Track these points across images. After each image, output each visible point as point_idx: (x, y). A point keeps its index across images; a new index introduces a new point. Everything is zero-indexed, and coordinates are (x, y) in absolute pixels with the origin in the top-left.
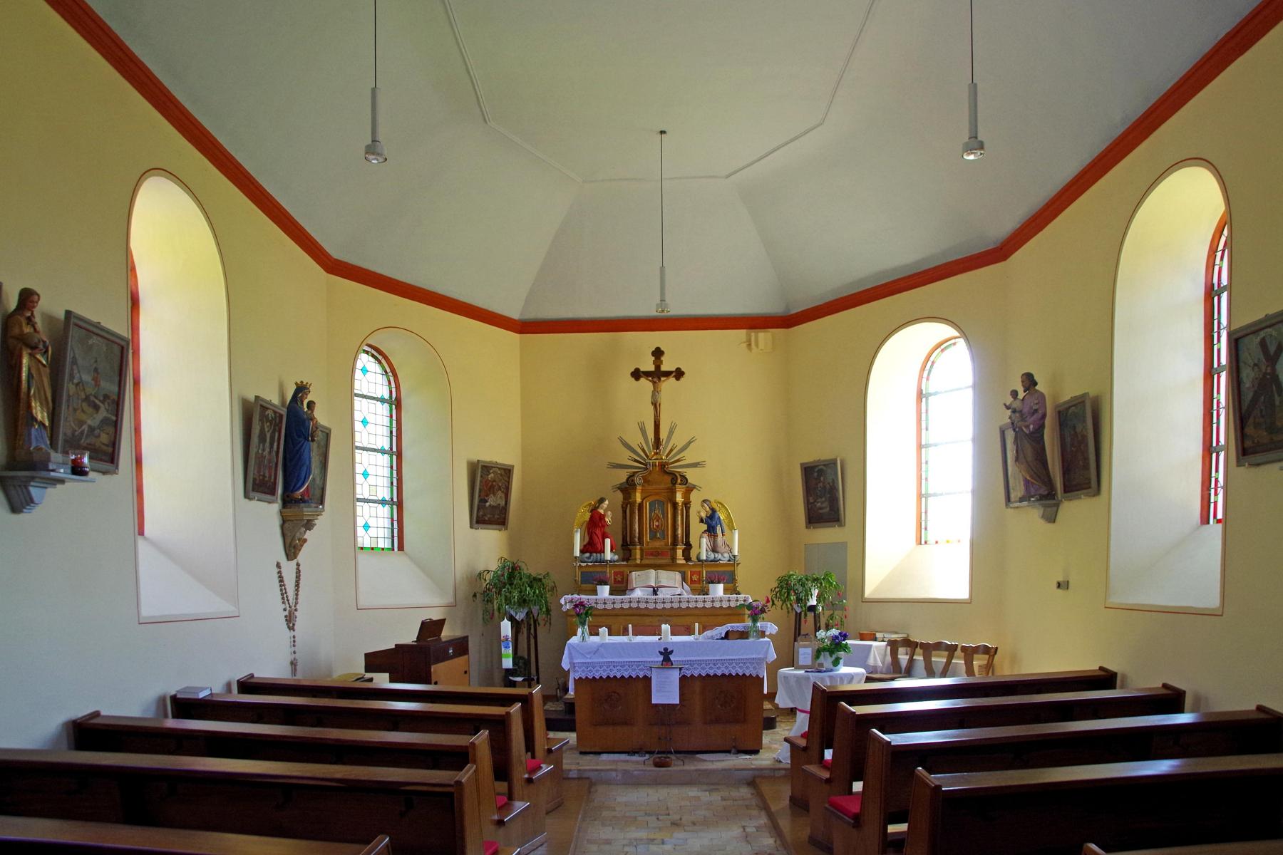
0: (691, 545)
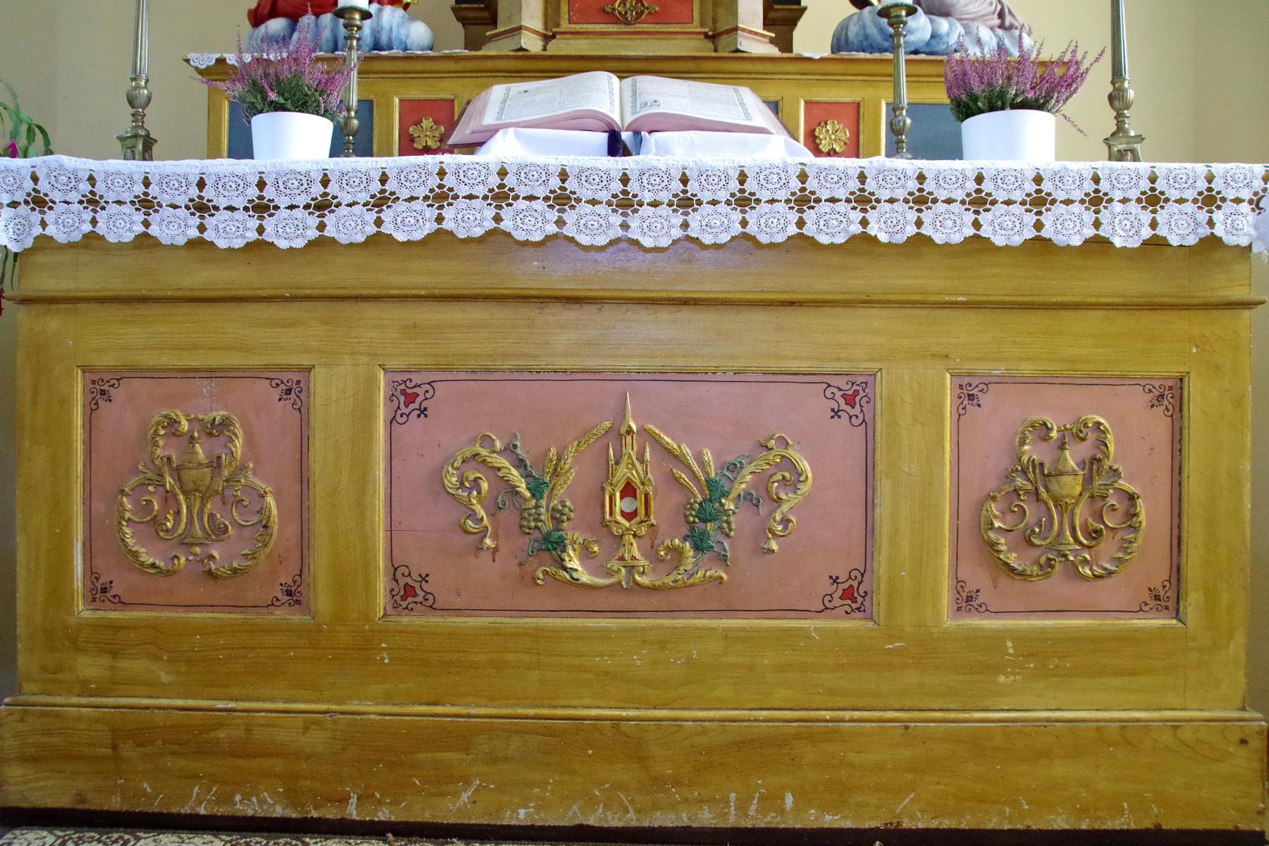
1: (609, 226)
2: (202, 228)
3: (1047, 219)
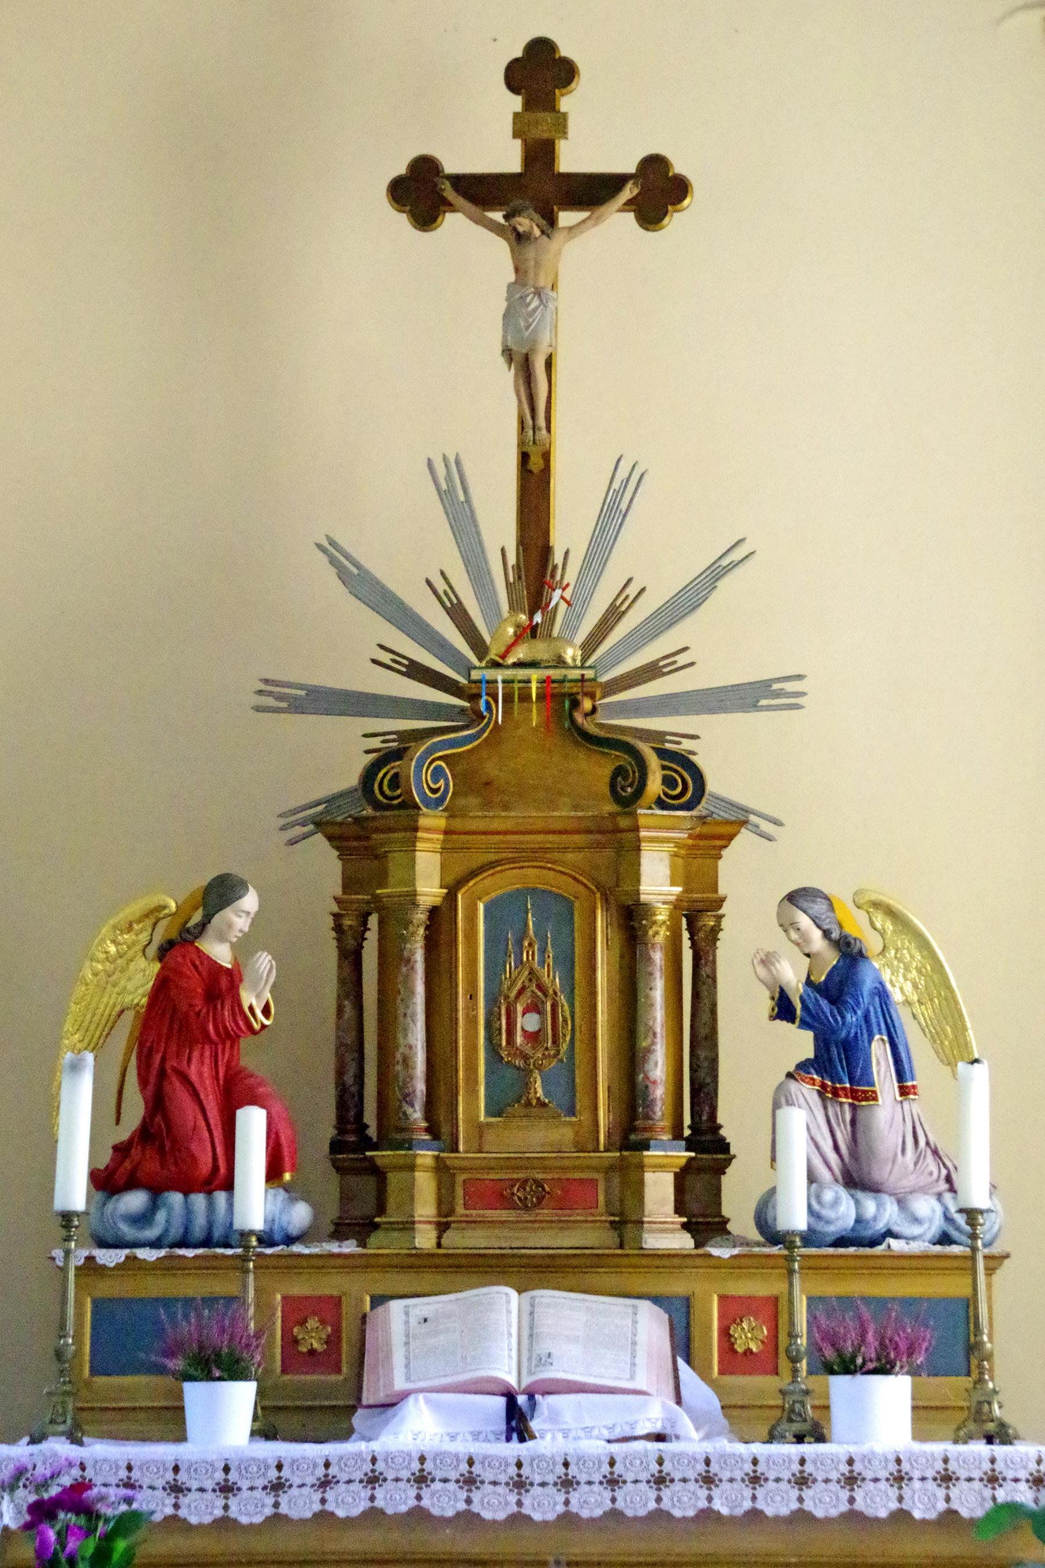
0: (724, 1147)
1: (507, 1503)
2: (176, 1506)
3: (859, 1495)
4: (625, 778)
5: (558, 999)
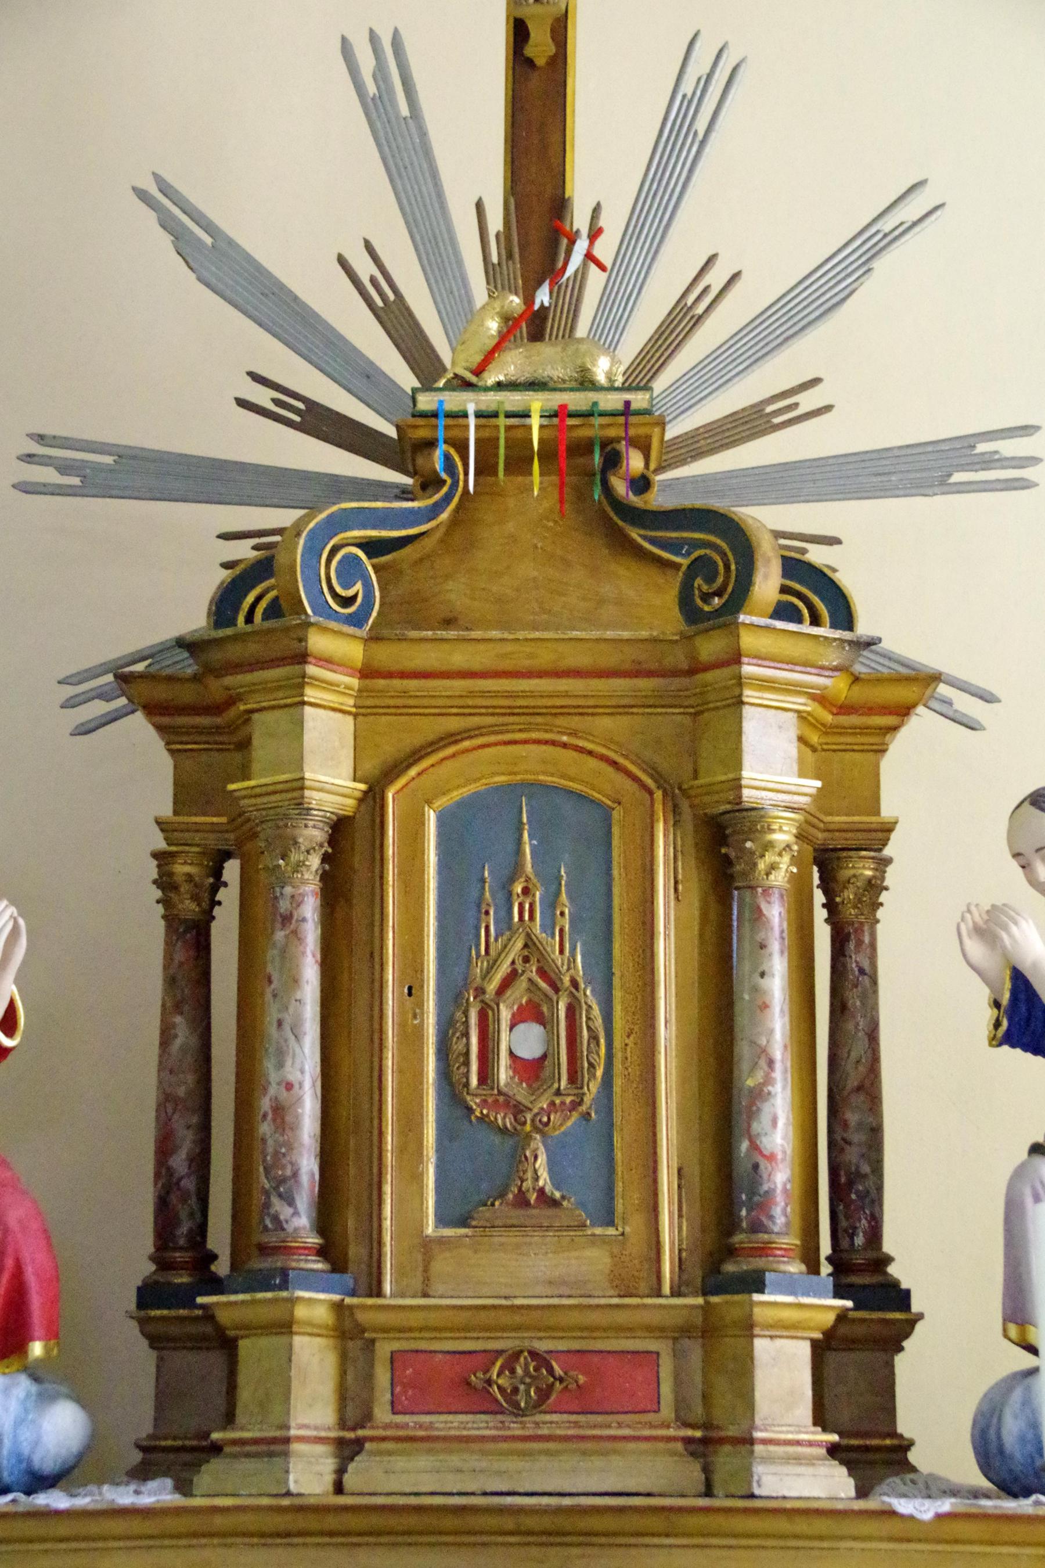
0: (901, 1298)
4: (710, 579)
5: (580, 995)
